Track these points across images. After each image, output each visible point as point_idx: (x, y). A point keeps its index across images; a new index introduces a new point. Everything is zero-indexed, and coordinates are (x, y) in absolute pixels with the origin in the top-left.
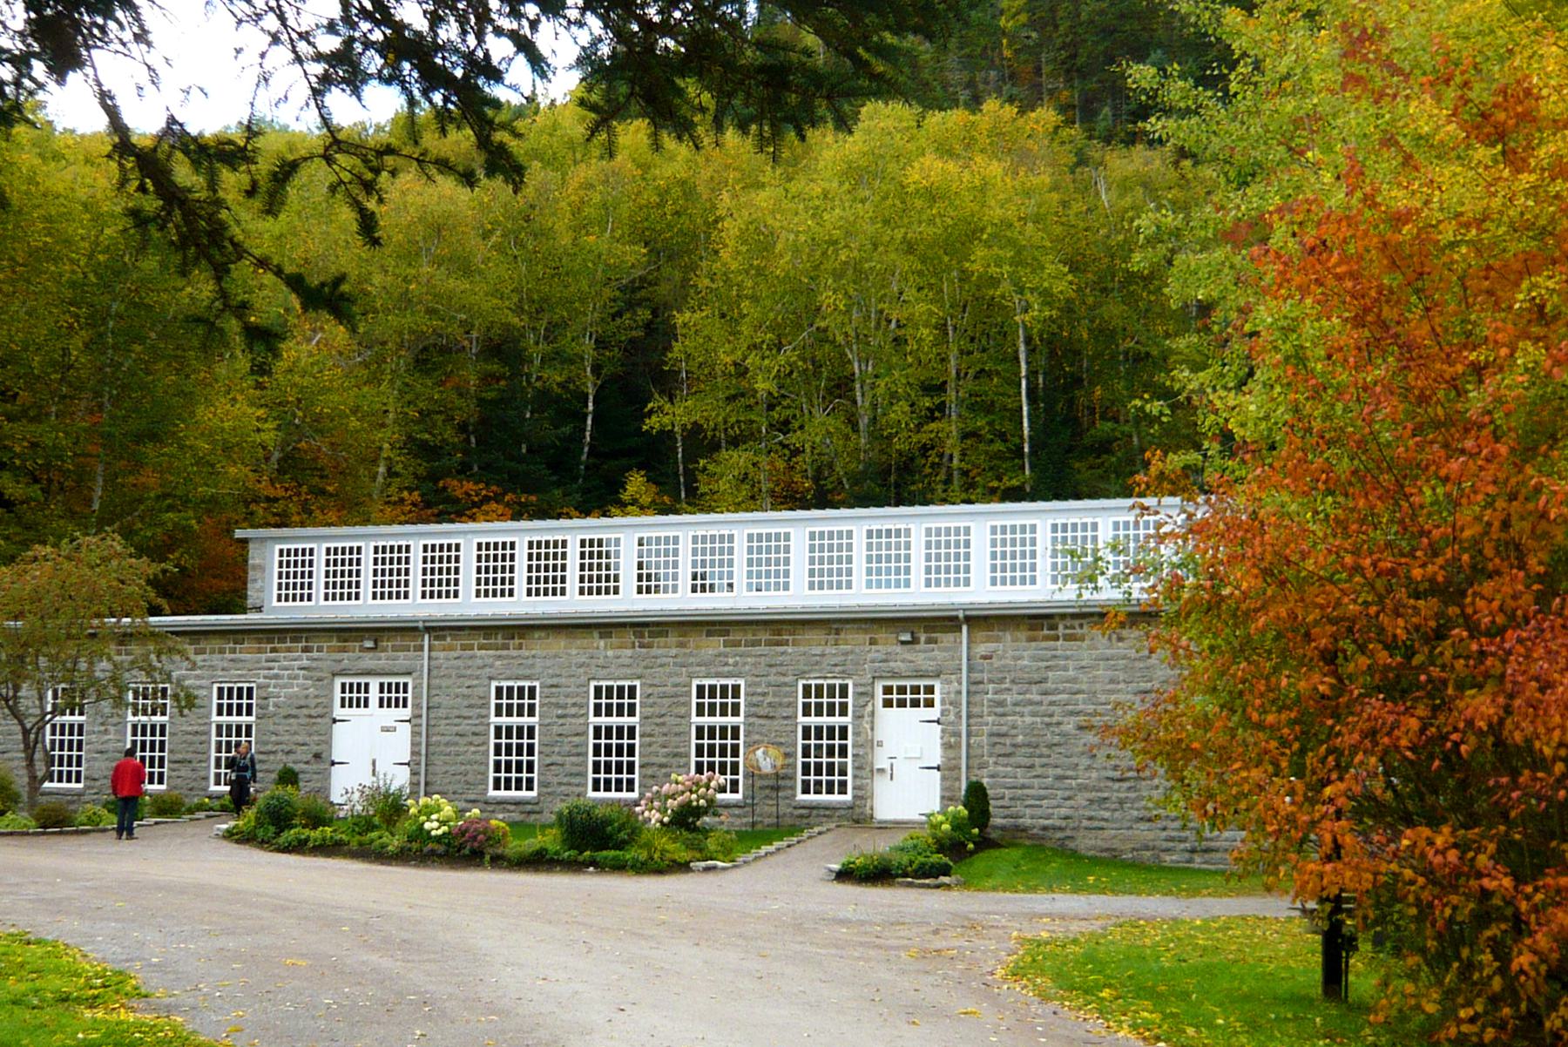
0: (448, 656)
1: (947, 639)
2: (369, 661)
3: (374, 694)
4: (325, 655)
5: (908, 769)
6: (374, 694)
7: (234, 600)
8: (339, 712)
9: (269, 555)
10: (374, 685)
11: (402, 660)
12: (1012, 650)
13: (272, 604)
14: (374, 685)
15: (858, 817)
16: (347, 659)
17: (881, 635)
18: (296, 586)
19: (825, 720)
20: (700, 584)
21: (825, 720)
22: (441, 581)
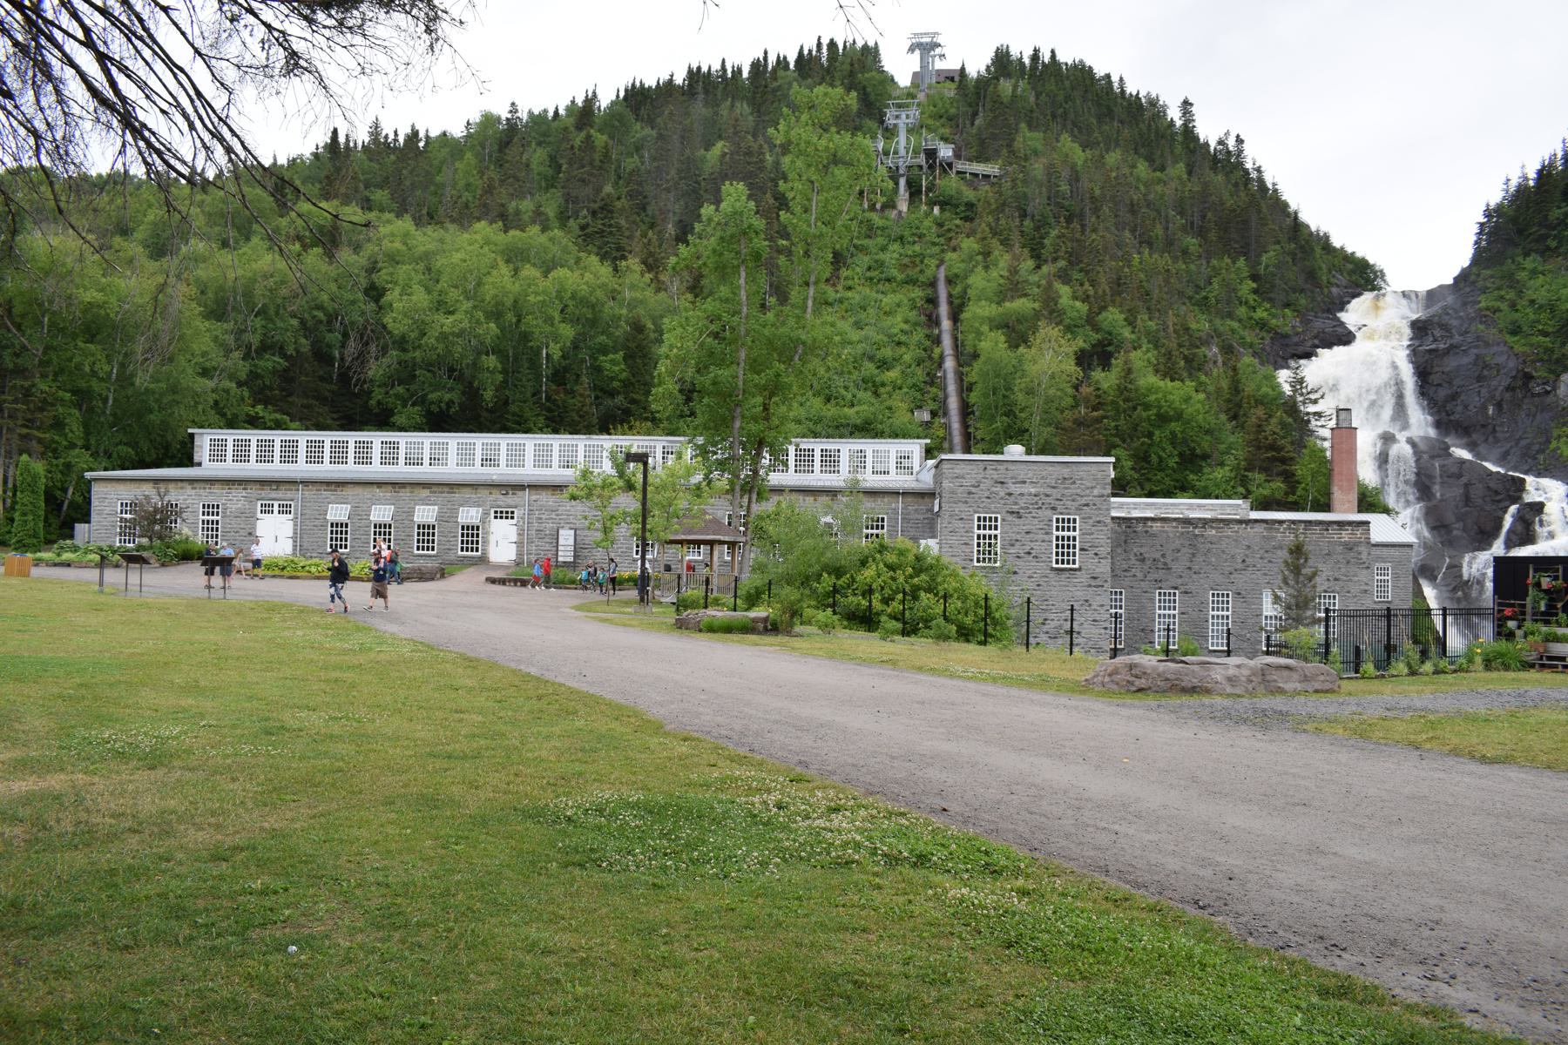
0: (310, 493)
1: (520, 493)
2: (274, 494)
3: (276, 508)
4: (254, 491)
5: (502, 543)
6: (276, 508)
7: (187, 459)
8: (259, 515)
9: (204, 441)
10: (276, 504)
11: (289, 495)
12: (546, 498)
13: (208, 466)
14: (276, 504)
15: (483, 560)
16: (263, 494)
17: (494, 491)
18: (218, 454)
19: (1066, 533)
20: (394, 446)
21: (1066, 533)
22: (289, 454)
